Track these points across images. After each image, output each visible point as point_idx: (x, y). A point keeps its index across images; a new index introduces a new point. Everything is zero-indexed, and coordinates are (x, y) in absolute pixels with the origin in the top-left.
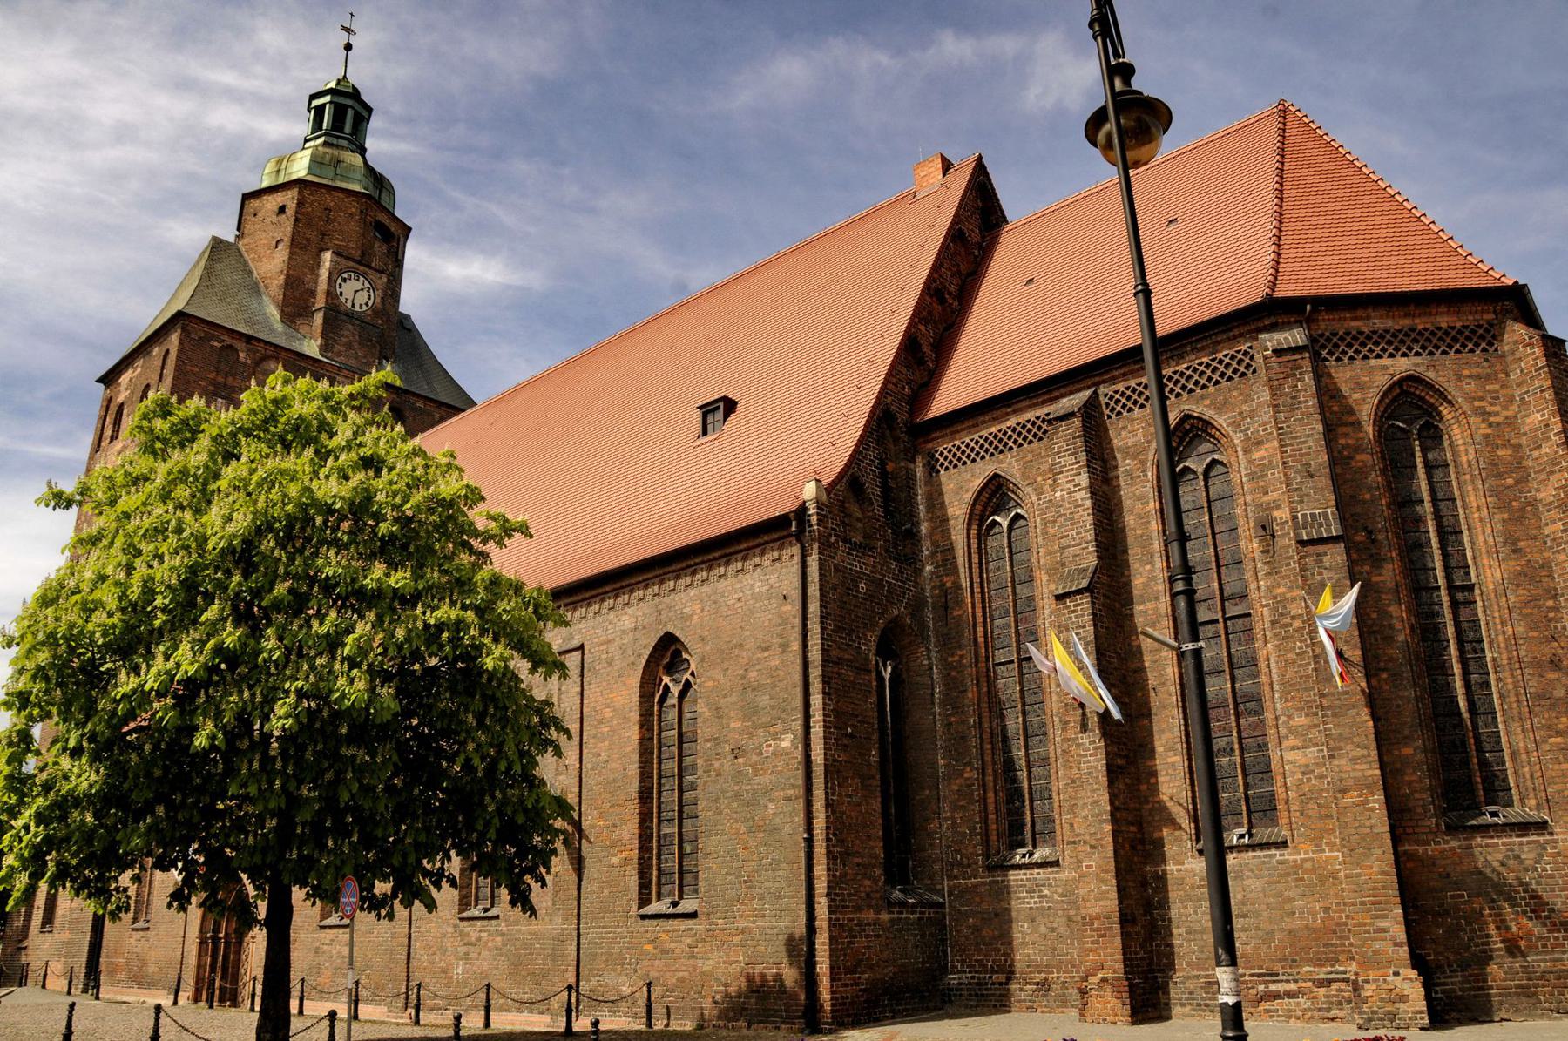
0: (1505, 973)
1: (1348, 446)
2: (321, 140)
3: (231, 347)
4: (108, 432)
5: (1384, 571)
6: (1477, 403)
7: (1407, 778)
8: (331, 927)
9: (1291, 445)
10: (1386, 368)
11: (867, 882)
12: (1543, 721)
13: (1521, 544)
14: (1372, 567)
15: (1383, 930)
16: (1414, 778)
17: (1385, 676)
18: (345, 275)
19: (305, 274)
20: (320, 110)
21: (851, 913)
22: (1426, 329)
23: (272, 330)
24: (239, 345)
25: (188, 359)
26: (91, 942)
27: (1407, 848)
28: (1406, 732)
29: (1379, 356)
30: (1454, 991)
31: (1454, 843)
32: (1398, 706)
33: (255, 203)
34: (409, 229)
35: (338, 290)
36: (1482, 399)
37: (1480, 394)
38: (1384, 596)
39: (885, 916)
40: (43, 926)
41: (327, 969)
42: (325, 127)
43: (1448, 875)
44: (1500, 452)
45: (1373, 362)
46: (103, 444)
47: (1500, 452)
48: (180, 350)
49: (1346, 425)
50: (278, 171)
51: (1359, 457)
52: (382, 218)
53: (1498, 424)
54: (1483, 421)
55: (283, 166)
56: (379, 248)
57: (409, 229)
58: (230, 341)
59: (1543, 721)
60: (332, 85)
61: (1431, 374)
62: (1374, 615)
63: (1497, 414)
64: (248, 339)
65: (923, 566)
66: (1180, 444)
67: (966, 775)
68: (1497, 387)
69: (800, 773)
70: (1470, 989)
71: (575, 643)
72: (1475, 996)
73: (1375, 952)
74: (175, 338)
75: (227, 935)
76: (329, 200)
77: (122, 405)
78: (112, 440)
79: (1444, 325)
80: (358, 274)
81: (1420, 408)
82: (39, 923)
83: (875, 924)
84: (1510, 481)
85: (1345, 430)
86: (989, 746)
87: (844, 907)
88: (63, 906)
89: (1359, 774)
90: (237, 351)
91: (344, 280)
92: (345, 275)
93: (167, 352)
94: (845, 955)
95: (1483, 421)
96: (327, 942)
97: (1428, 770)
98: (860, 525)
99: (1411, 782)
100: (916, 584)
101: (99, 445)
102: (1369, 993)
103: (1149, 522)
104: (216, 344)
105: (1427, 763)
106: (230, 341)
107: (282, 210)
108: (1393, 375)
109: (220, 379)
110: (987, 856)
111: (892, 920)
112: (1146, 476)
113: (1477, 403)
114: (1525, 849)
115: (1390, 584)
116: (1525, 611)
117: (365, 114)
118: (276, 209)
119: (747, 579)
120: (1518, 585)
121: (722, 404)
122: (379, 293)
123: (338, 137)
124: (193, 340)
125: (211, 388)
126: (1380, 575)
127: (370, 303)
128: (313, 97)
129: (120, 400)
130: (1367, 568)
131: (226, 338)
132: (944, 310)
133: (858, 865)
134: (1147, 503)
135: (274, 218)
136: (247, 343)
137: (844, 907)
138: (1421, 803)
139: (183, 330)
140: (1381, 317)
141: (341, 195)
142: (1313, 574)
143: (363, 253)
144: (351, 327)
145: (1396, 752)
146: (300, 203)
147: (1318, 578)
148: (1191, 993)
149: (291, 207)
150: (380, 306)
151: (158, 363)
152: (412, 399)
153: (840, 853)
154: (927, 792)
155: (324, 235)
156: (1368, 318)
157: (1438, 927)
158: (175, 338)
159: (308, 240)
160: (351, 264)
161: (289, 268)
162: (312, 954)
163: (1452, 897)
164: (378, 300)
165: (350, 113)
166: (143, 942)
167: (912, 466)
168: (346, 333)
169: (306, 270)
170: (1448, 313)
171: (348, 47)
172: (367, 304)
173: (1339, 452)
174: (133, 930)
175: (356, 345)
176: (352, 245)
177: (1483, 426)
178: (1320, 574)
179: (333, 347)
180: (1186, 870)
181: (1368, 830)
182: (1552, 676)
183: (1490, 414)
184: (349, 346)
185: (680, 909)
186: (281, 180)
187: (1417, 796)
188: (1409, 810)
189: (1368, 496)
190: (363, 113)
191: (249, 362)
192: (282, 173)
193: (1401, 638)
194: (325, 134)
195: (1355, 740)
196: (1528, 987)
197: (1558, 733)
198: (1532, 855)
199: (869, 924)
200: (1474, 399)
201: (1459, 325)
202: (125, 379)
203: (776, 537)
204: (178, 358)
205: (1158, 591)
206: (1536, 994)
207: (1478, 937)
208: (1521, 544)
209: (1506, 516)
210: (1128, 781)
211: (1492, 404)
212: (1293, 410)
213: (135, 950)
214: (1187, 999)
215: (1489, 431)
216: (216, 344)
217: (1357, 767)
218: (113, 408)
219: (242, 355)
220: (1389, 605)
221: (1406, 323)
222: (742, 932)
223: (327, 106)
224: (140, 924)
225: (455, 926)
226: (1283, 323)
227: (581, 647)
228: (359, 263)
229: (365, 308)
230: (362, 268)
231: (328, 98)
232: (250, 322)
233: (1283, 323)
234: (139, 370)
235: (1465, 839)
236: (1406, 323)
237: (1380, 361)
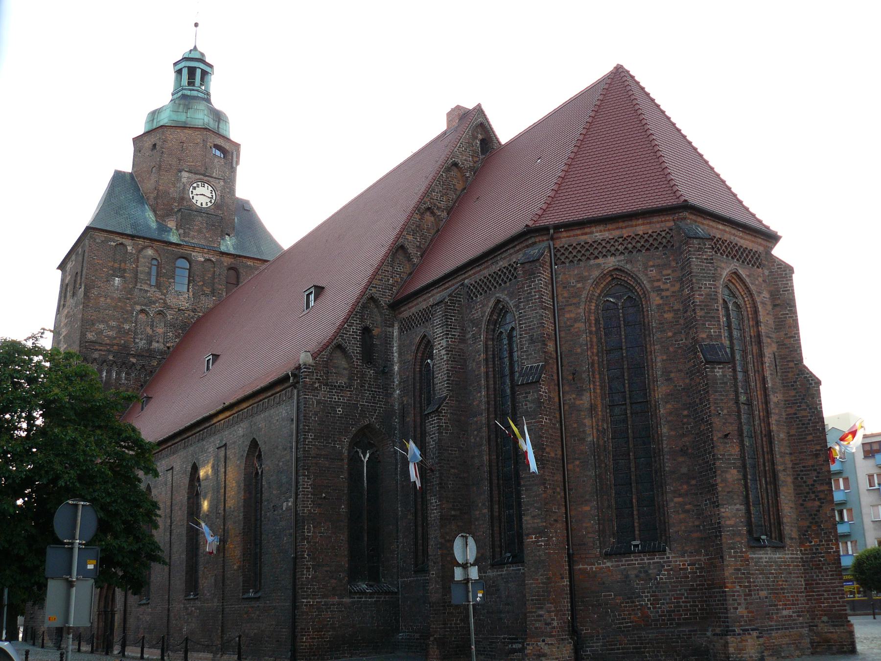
0: (628, 640)
1: (571, 318)
3: (122, 244)
5: (584, 398)
6: (656, 284)
7: (584, 525)
9: (525, 323)
10: (599, 265)
11: (333, 581)
12: (672, 488)
13: (672, 375)
14: (577, 395)
15: (541, 616)
16: (589, 525)
17: (577, 462)
18: (195, 185)
19: (170, 189)
21: (319, 598)
22: (629, 236)
23: (149, 228)
27: (581, 566)
28: (587, 497)
29: (597, 258)
30: (597, 650)
31: (609, 564)
32: (584, 481)
35: (191, 196)
36: (658, 280)
37: (658, 277)
38: (582, 413)
39: (346, 600)
43: (604, 583)
44: (666, 316)
45: (592, 262)
47: (666, 316)
49: (571, 305)
50: (153, 120)
51: (576, 325)
53: (667, 297)
54: (658, 294)
55: (156, 117)
59: (672, 488)
61: (628, 266)
62: (575, 425)
63: (668, 290)
64: (132, 237)
65: (395, 391)
66: (498, 317)
67: (409, 517)
68: (669, 272)
70: (607, 650)
72: (609, 654)
73: (536, 628)
76: (183, 135)
79: (641, 233)
80: (204, 182)
81: (626, 287)
83: (339, 605)
84: (670, 334)
85: (569, 308)
86: (420, 500)
87: (315, 595)
89: (536, 525)
91: (194, 188)
94: (313, 622)
95: (658, 294)
97: (599, 520)
98: (346, 372)
99: (586, 528)
100: (387, 403)
102: (529, 651)
103: (480, 367)
104: (112, 243)
105: (598, 516)
108: (603, 270)
109: (116, 265)
110: (416, 565)
111: (353, 603)
112: (480, 337)
113: (656, 284)
114: (652, 567)
115: (587, 405)
116: (669, 418)
117: (208, 69)
118: (151, 146)
120: (666, 403)
121: (313, 290)
122: (218, 193)
124: (98, 243)
125: (111, 272)
126: (582, 400)
128: (175, 64)
130: (574, 396)
131: (118, 239)
132: (435, 220)
133: (327, 571)
134: (480, 355)
137: (315, 595)
138: (592, 539)
140: (601, 231)
142: (522, 405)
145: (580, 509)
147: (525, 407)
148: (484, 648)
152: (245, 260)
153: (312, 565)
154: (391, 527)
155: (180, 160)
156: (592, 233)
157: (595, 614)
159: (170, 165)
160: (198, 177)
163: (605, 596)
165: (198, 72)
167: (391, 329)
168: (197, 223)
169: (170, 185)
170: (643, 224)
172: (211, 202)
173: (565, 323)
175: (204, 231)
176: (198, 164)
177: (657, 298)
178: (526, 405)
180: (488, 576)
181: (538, 558)
182: (681, 459)
183: (662, 290)
184: (200, 231)
187: (590, 535)
188: (584, 544)
189: (579, 350)
192: (155, 121)
193: (590, 439)
195: (535, 505)
196: (640, 648)
197: (680, 496)
198: (655, 571)
199: (334, 605)
200: (654, 281)
201: (650, 232)
205: (483, 409)
206: (644, 652)
207: (617, 620)
208: (672, 375)
209: (665, 358)
210: (460, 524)
211: (665, 283)
212: (528, 301)
214: (483, 651)
215: (661, 302)
216: (112, 243)
217: (535, 521)
219: (129, 248)
220: (585, 418)
221: (616, 233)
222: (274, 609)
225: (184, 604)
226: (539, 241)
228: (204, 175)
229: (209, 204)
233: (539, 241)
235: (616, 561)
236: (616, 233)
237: (597, 261)
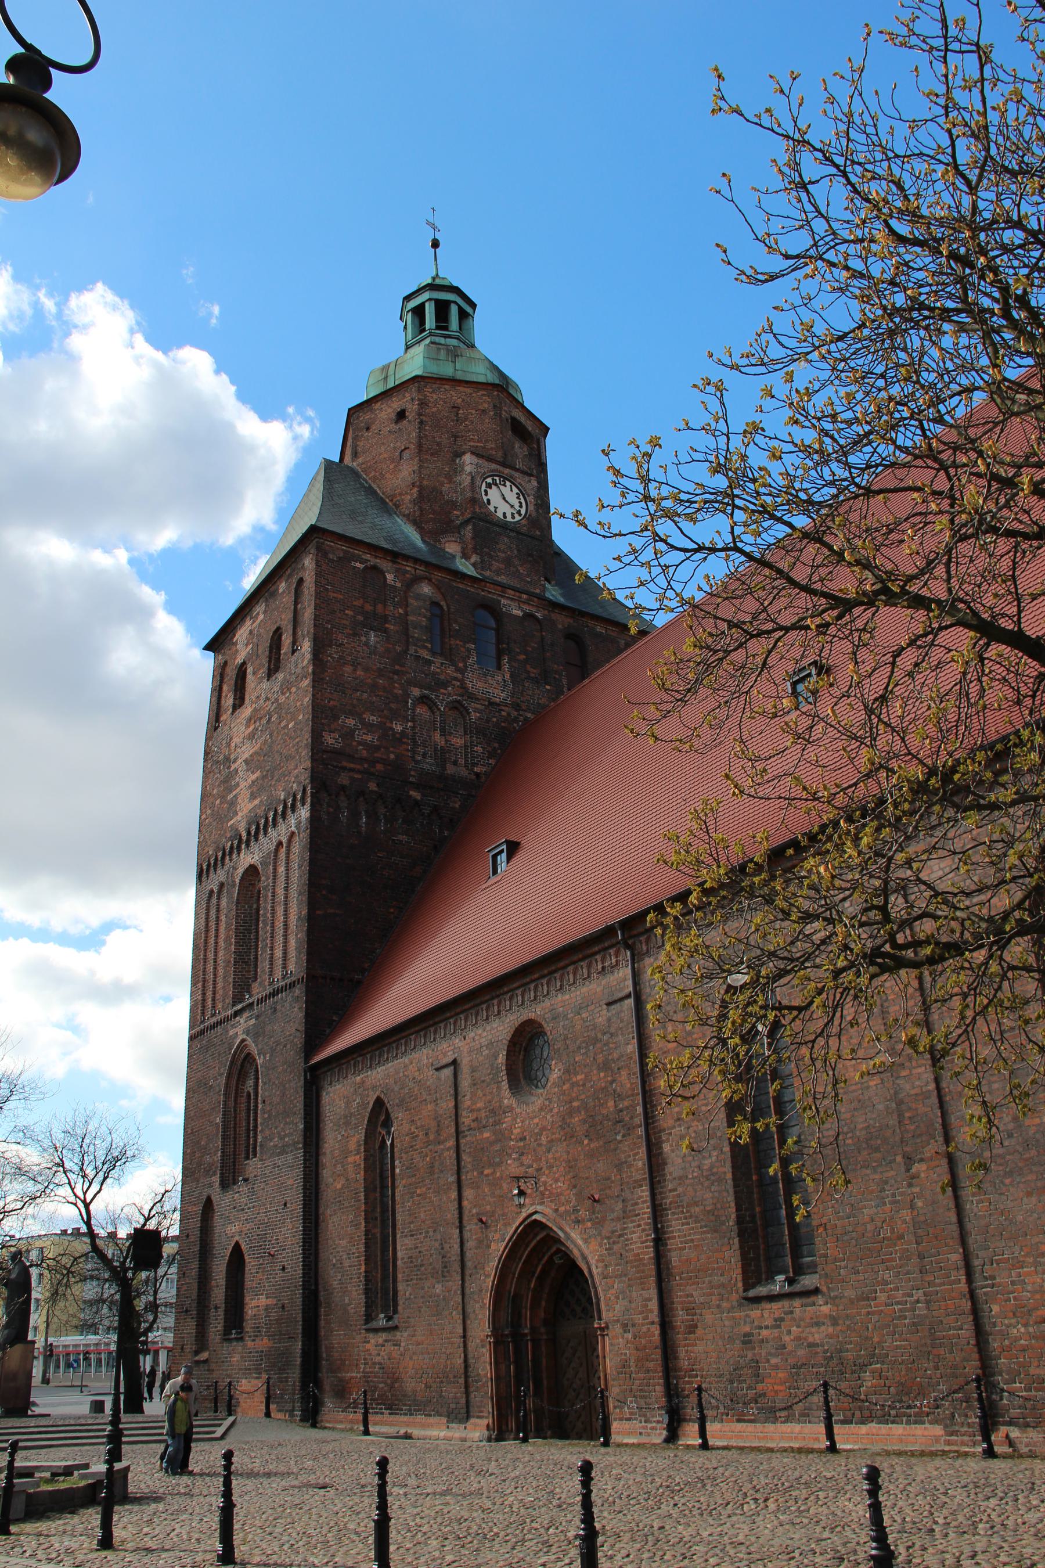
2: (427, 341)
3: (375, 568)
4: (228, 701)
8: (772, 1298)
18: (489, 480)
19: (442, 484)
20: (419, 312)
24: (385, 565)
25: (329, 583)
26: (303, 1349)
33: (365, 417)
34: (548, 429)
35: (485, 498)
40: (227, 1331)
41: (776, 1367)
42: (427, 326)
46: (223, 718)
48: (319, 574)
52: (517, 414)
56: (519, 449)
57: (548, 429)
58: (373, 561)
60: (429, 281)
69: (456, 1212)
71: (449, 1059)
74: (308, 562)
75: (532, 1328)
76: (456, 396)
77: (244, 663)
78: (235, 708)
82: (220, 1327)
88: (254, 1303)
90: (382, 573)
91: (489, 486)
92: (489, 480)
93: (301, 581)
96: (768, 1322)
101: (217, 720)
104: (358, 565)
106: (373, 561)
107: (401, 415)
109: (368, 607)
117: (469, 309)
118: (393, 416)
119: (415, 1055)
121: (504, 847)
122: (530, 499)
123: (446, 337)
125: (360, 618)
127: (523, 511)
128: (408, 298)
129: (239, 660)
135: (393, 427)
136: (394, 562)
139: (319, 548)
141: (469, 391)
143: (505, 455)
144: (506, 540)
146: (423, 404)
149: (412, 409)
150: (534, 514)
151: (288, 600)
152: (591, 623)
155: (456, 437)
158: (308, 562)
159: (439, 444)
160: (494, 466)
161: (421, 479)
162: (738, 1345)
164: (531, 508)
165: (454, 310)
166: (389, 1347)
168: (502, 547)
171: (435, 244)
172: (519, 513)
174: (368, 1330)
175: (516, 562)
176: (490, 445)
179: (491, 565)
185: (797, 1288)
186: (391, 384)
190: (467, 309)
191: (398, 585)
194: (431, 335)
202: (242, 634)
203: (581, 956)
204: (317, 583)
213: (378, 1359)
216: (358, 565)
218: (231, 672)
219: (390, 577)
223: (427, 305)
224: (381, 1321)
227: (454, 1062)
228: (504, 465)
229: (518, 518)
230: (507, 471)
231: (426, 296)
232: (389, 539)
234: (261, 617)
